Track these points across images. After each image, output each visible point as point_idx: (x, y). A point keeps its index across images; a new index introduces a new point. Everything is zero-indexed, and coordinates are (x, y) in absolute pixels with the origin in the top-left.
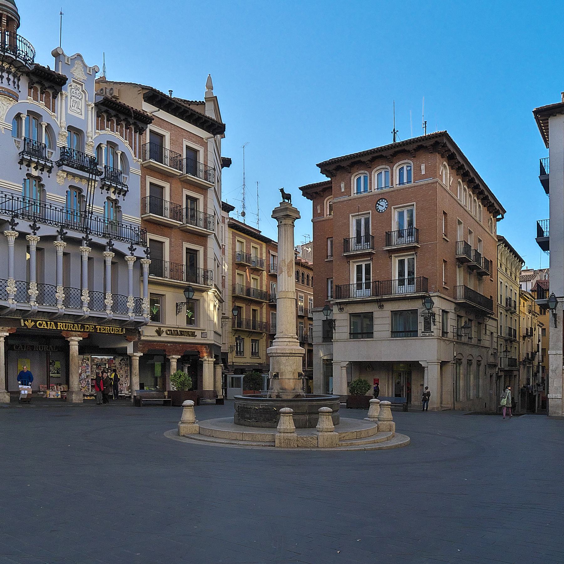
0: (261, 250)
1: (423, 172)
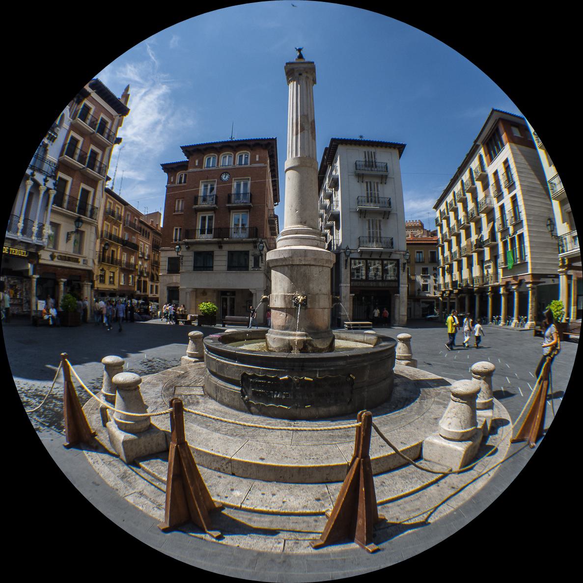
0: (121, 210)
1: (257, 159)
